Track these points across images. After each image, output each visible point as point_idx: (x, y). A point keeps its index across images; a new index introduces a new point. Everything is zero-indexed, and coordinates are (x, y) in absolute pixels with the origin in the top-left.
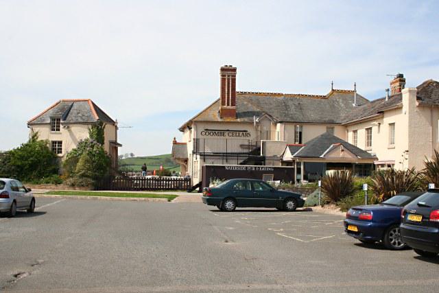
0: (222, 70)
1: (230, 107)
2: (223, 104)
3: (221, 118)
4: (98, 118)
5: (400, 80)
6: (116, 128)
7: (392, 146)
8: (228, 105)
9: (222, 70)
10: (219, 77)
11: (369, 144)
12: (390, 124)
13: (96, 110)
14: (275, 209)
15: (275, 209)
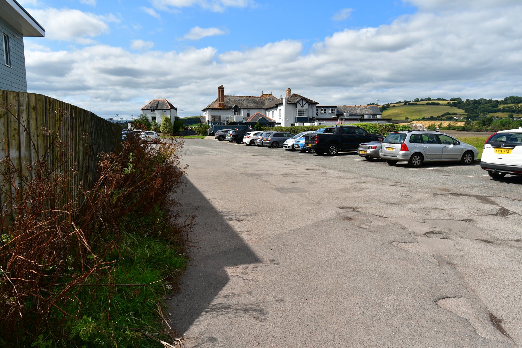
0: (219, 88)
1: (222, 103)
2: (219, 101)
3: (219, 107)
4: (170, 107)
5: (289, 90)
6: (177, 111)
7: (280, 118)
8: (221, 102)
9: (219, 88)
10: (218, 91)
11: (273, 117)
12: (280, 110)
13: (438, 100)
14: (316, 154)
15: (316, 154)
